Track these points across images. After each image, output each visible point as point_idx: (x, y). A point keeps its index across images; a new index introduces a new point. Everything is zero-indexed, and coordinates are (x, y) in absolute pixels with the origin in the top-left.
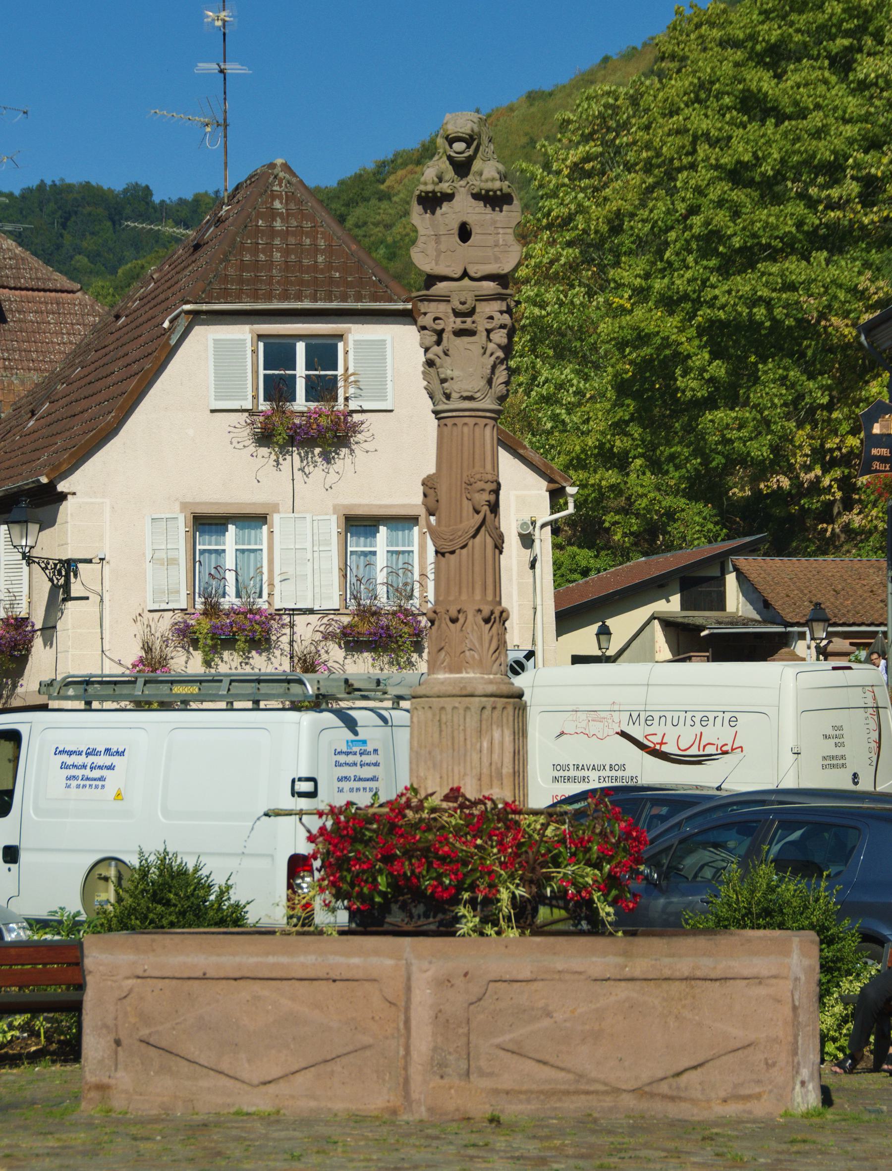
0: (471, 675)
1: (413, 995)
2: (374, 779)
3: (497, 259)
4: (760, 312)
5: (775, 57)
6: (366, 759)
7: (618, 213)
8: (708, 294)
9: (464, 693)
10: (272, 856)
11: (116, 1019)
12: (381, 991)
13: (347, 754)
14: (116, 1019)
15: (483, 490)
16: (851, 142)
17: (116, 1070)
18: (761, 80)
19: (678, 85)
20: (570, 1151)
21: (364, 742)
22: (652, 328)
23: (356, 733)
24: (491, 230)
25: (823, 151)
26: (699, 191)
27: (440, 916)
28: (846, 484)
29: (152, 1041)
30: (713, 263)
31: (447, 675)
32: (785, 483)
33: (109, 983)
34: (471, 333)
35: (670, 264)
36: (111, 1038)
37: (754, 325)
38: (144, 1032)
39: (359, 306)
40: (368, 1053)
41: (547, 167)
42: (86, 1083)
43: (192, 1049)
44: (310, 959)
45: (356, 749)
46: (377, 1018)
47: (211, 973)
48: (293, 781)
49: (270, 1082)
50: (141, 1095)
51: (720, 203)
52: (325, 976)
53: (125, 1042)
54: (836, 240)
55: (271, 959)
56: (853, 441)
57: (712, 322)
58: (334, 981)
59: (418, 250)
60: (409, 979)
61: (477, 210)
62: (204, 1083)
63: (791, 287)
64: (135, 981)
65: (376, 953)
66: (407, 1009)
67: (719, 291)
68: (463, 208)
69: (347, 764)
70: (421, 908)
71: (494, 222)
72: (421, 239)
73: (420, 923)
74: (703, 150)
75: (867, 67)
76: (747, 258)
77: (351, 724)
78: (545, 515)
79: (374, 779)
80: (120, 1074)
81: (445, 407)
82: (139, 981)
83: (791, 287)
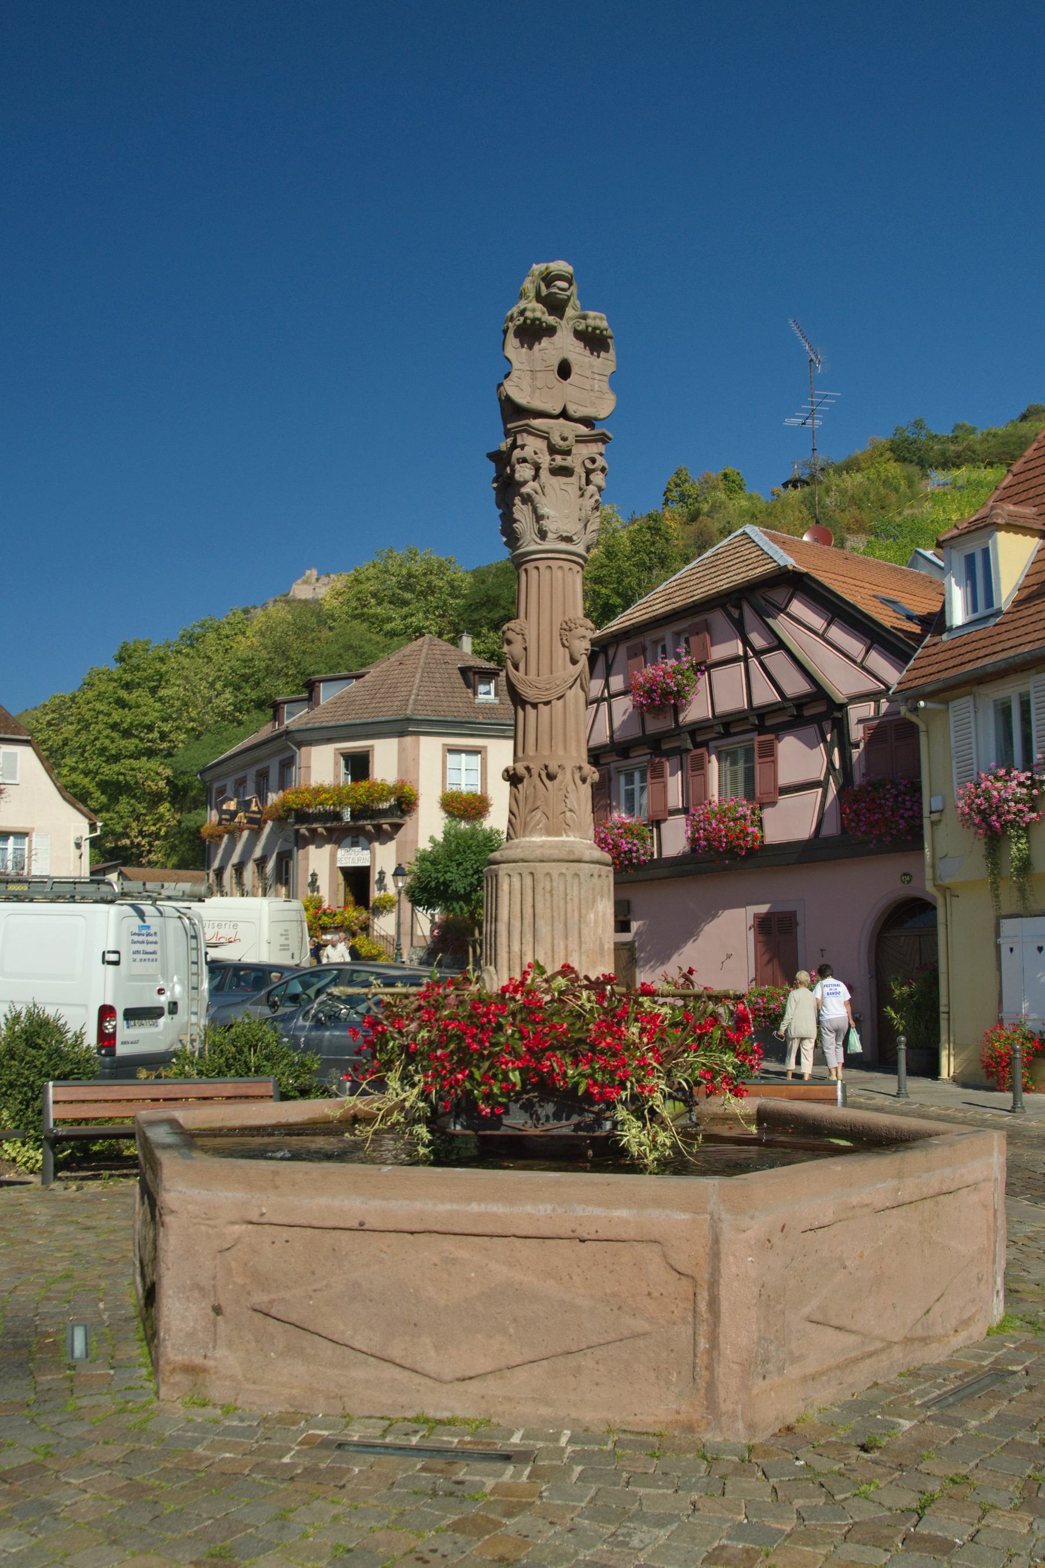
0: (572, 839)
1: (723, 1266)
2: (154, 953)
3: (593, 404)
4: (121, 778)
5: (128, 686)
6: (150, 939)
7: (67, 738)
8: (101, 770)
9: (572, 858)
10: (86, 1006)
11: (214, 1278)
12: (665, 1256)
13: (139, 935)
14: (214, 1278)
15: (584, 637)
16: (157, 718)
17: (214, 1347)
18: (123, 694)
19: (90, 694)
20: (888, 1464)
21: (149, 927)
22: (79, 781)
23: (144, 921)
24: (588, 373)
25: (147, 721)
26: (100, 732)
27: (575, 1119)
28: (150, 844)
29: (273, 1312)
30: (104, 759)
31: (544, 838)
32: (128, 842)
33: (203, 1228)
34: (565, 472)
35: (86, 758)
36: (207, 1304)
37: (118, 782)
38: (260, 1298)
39: (7, 736)
40: (641, 1343)
41: (37, 721)
42: (168, 1363)
43: (340, 1328)
44: (544, 1209)
45: (144, 932)
46: (656, 1294)
47: (371, 1222)
48: (104, 953)
49: (471, 1378)
50: (254, 1383)
51: (107, 737)
52: (571, 1234)
53: (227, 1309)
54: (150, 753)
55: (475, 1207)
56: (153, 828)
57: (101, 780)
58: (583, 1241)
59: (512, 384)
60: (716, 1241)
61: (577, 350)
62: (359, 1373)
63: (133, 769)
64: (244, 1226)
65: (658, 1202)
66: (714, 1284)
67: (106, 769)
68: (564, 344)
69: (139, 942)
70: (550, 1108)
71: (591, 366)
72: (514, 374)
73: (548, 1126)
74: (101, 717)
75: (162, 693)
76: (116, 758)
77: (141, 914)
78: (86, 834)
79: (154, 953)
80: (221, 1352)
81: (540, 547)
82: (250, 1226)
83: (133, 769)
